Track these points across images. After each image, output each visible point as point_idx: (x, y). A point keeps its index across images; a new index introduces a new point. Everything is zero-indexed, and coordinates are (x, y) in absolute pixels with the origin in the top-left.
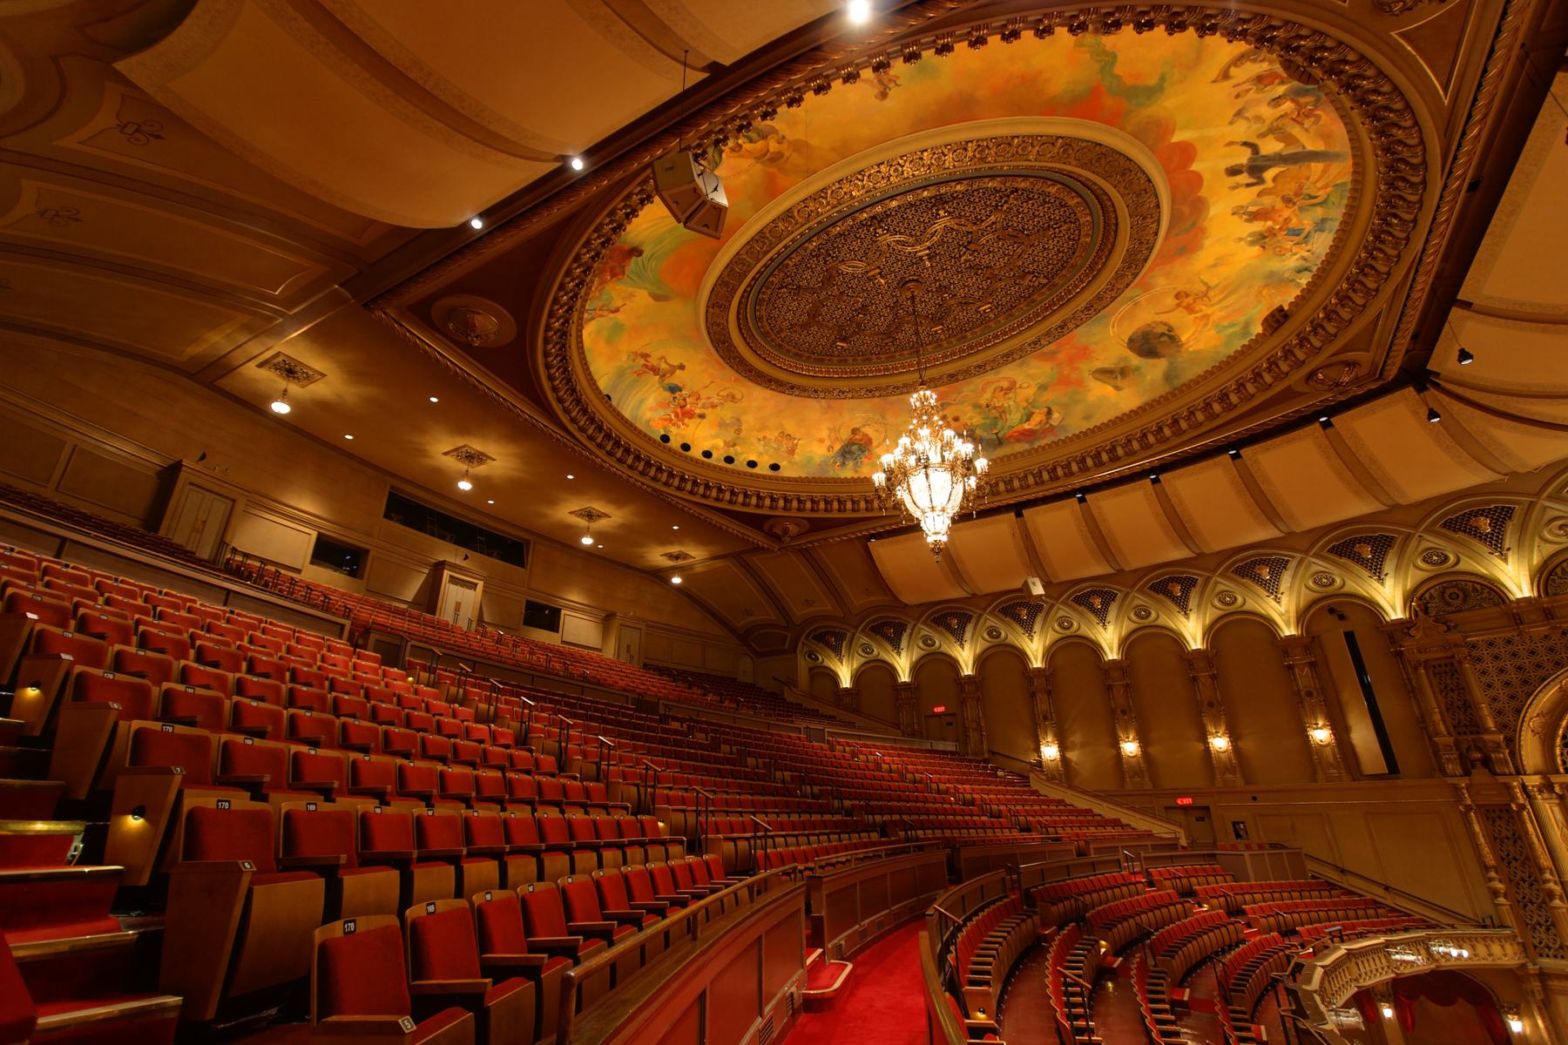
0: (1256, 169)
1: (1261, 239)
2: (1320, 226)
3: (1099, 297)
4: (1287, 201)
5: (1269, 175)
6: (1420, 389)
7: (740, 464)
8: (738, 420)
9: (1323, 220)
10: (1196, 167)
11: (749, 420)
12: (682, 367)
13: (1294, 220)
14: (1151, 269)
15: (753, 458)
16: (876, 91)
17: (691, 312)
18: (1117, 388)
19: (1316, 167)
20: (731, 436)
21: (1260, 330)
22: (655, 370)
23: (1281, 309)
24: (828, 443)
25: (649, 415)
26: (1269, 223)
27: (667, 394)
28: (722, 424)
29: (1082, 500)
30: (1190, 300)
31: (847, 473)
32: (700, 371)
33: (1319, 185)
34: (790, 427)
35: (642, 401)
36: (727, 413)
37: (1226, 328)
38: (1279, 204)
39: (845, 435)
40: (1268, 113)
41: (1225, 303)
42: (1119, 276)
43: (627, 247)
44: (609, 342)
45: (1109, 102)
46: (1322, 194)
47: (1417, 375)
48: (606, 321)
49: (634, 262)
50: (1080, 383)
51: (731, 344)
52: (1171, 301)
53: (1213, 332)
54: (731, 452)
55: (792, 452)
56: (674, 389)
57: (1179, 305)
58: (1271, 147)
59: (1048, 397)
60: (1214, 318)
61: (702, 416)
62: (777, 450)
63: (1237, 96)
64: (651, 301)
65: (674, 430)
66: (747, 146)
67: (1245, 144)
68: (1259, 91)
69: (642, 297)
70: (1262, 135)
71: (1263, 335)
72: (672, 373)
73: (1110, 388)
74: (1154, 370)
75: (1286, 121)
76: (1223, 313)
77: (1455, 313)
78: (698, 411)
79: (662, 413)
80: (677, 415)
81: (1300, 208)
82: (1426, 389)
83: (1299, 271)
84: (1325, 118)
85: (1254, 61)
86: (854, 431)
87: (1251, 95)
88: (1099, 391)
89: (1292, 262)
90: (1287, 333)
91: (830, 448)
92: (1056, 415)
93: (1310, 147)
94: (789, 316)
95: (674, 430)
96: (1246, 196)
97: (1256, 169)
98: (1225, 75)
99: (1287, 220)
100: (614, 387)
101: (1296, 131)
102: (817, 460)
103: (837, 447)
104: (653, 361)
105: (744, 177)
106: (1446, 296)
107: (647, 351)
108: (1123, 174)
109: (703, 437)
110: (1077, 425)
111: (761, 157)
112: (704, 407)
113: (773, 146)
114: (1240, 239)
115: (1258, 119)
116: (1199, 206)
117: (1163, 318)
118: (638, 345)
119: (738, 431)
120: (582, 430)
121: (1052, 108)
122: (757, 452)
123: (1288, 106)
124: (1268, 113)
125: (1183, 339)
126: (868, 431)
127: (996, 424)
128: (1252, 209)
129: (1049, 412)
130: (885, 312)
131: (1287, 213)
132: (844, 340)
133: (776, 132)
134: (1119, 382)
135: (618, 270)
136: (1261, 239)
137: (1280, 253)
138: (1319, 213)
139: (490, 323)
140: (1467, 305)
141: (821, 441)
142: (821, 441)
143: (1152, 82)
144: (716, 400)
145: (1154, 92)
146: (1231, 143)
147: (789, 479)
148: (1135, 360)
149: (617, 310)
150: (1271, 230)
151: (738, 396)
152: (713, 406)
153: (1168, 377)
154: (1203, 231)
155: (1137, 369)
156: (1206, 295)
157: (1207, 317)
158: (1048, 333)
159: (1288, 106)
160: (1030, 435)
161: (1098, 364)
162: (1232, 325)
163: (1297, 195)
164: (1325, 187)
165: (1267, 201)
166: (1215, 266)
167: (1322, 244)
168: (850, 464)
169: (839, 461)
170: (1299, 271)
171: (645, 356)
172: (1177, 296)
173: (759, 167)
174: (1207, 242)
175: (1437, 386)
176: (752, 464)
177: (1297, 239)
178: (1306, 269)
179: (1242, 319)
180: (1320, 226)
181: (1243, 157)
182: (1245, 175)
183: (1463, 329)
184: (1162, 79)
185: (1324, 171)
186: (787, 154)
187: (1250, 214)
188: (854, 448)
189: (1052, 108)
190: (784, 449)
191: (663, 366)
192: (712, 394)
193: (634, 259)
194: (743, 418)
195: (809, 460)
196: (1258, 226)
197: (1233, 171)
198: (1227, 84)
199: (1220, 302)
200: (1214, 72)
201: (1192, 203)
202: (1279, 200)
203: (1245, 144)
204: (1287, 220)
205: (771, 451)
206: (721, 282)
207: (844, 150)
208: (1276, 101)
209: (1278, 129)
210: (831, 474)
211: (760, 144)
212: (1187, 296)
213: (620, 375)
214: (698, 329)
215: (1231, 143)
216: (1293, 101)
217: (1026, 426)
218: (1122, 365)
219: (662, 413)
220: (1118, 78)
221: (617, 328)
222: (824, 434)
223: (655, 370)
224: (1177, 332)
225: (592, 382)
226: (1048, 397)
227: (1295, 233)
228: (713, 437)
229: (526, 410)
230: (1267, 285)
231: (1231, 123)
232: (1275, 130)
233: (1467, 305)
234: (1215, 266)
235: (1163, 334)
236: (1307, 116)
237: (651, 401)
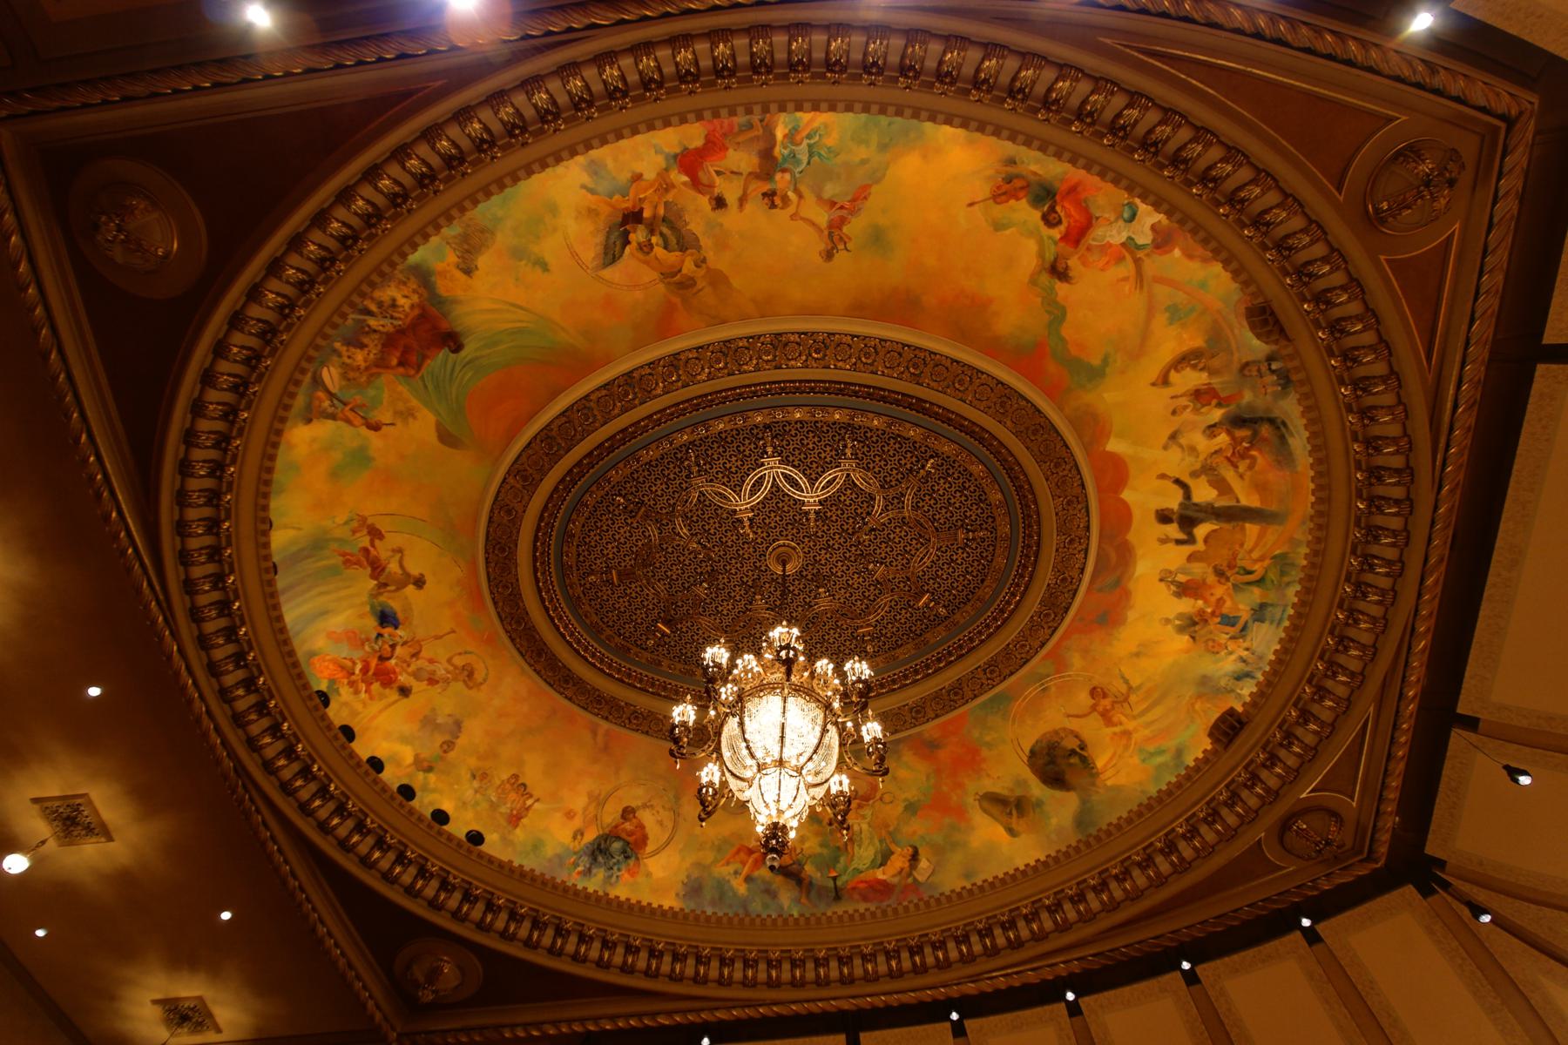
0: (1187, 519)
1: (1191, 625)
2: (1259, 613)
3: (1007, 652)
4: (1220, 573)
5: (1201, 531)
6: (1426, 891)
7: (424, 803)
8: (458, 725)
9: (1263, 606)
10: (1126, 495)
11: (475, 733)
12: (419, 583)
13: (1228, 604)
14: (1066, 636)
15: (447, 806)
16: (822, 246)
17: (473, 478)
18: (1011, 832)
19: (1252, 529)
20: (431, 747)
21: (1207, 744)
22: (377, 568)
23: (1231, 712)
24: (577, 823)
25: (320, 643)
26: (1200, 602)
27: (371, 623)
28: (428, 722)
29: (958, 1030)
30: (1106, 703)
31: (593, 884)
32: (441, 599)
33: (1255, 555)
34: (533, 774)
35: (324, 613)
36: (446, 702)
37: (1152, 755)
38: (1211, 579)
39: (611, 815)
40: (1204, 445)
41: (1150, 716)
42: (1033, 627)
43: (444, 326)
44: (335, 474)
45: (1051, 367)
46: (1258, 568)
47: (1414, 868)
48: (349, 435)
49: (440, 359)
50: (960, 812)
51: (513, 552)
52: (1083, 699)
53: (1136, 760)
54: (417, 780)
55: (515, 819)
56: (386, 618)
57: (1094, 708)
58: (1204, 493)
59: (917, 828)
60: (1136, 737)
61: (405, 691)
62: (493, 806)
63: (1174, 413)
64: (432, 437)
65: (345, 692)
66: (659, 251)
67: (1177, 481)
68: (1196, 411)
69: (424, 425)
70: (1195, 474)
71: (1215, 752)
72: (401, 585)
73: (1001, 830)
74: (1061, 809)
75: (1219, 459)
76: (1147, 732)
77: (1458, 739)
78: (403, 679)
79: (344, 652)
80: (365, 670)
81: (1234, 586)
82: (1433, 892)
83: (1238, 678)
84: (1260, 461)
85: (1194, 367)
86: (628, 813)
87: (1187, 415)
88: (986, 831)
89: (1228, 665)
90: (1248, 740)
91: (578, 833)
92: (923, 864)
93: (1244, 502)
94: (610, 550)
95: (345, 692)
96: (1175, 557)
97: (1187, 519)
98: (1164, 381)
99: (1220, 601)
100: (296, 558)
101: (1229, 474)
102: (549, 851)
103: (591, 836)
104: (382, 550)
105: (639, 295)
106: (1441, 716)
107: (383, 525)
108: (1056, 466)
109: (387, 732)
110: (951, 881)
111: (669, 274)
112: (416, 675)
113: (688, 267)
114: (1168, 621)
115: (1192, 450)
116: (1125, 555)
117: (1073, 724)
118: (373, 508)
119: (448, 746)
120: (184, 558)
121: (994, 349)
122: (458, 800)
123: (1223, 439)
124: (1204, 445)
125: (1100, 763)
126: (647, 818)
127: (836, 860)
128: (1181, 578)
129: (915, 857)
130: (739, 592)
131: (1220, 591)
132: (667, 623)
133: (699, 248)
134: (1014, 822)
135: (414, 358)
136: (1191, 625)
137: (1214, 649)
138: (1256, 595)
139: (161, 235)
140: (1471, 723)
141: (570, 815)
142: (570, 815)
143: (1096, 361)
144: (441, 672)
145: (1096, 374)
146: (1163, 476)
147: (491, 860)
148: (1037, 789)
149: (376, 427)
150: (1201, 612)
151: (479, 676)
152: (432, 681)
153: (1081, 821)
154: (1127, 594)
155: (1039, 804)
156: (1126, 700)
157: (1127, 734)
158: (937, 696)
159: (1223, 439)
160: (883, 889)
161: (989, 785)
162: (1161, 752)
163: (1231, 567)
164: (1261, 559)
165: (1200, 570)
166: (1137, 655)
167: (1266, 640)
168: (600, 874)
169: (585, 861)
170: (1238, 678)
171: (375, 534)
172: (1093, 692)
173: (661, 287)
174: (1131, 615)
175: (1446, 886)
176: (441, 817)
177: (1232, 631)
178: (1248, 675)
179: (1171, 744)
180: (1259, 613)
181: (1173, 500)
182: (1175, 526)
183: (1470, 766)
184: (1105, 361)
185: (1261, 536)
186: (700, 284)
187: (1179, 585)
188: (617, 845)
189: (994, 349)
190: (504, 809)
191: (393, 567)
192: (439, 655)
193: (443, 354)
194: (466, 724)
195: (537, 846)
196: (1187, 606)
197: (1164, 517)
198: (1167, 392)
199: (1143, 713)
200: (1153, 369)
201: (1121, 556)
202: (1210, 570)
203: (1177, 481)
204: (1220, 601)
205: (485, 805)
206: (545, 435)
207: (765, 307)
208: (1211, 430)
209: (1212, 469)
210: (561, 876)
211: (672, 257)
212: (1105, 696)
213: (317, 545)
214: (476, 520)
215: (1163, 476)
216: (1229, 433)
217: (880, 875)
218: (1019, 793)
219: (344, 652)
220: (1063, 340)
221: (360, 457)
222: (579, 802)
223: (377, 568)
224: (1091, 752)
225: (264, 526)
226: (917, 828)
227: (1229, 621)
228: (404, 740)
229: (107, 459)
230: (1200, 696)
231: (1165, 448)
232: (1207, 470)
233: (1471, 723)
234: (1137, 655)
235: (1073, 752)
236: (1243, 457)
237: (339, 621)
